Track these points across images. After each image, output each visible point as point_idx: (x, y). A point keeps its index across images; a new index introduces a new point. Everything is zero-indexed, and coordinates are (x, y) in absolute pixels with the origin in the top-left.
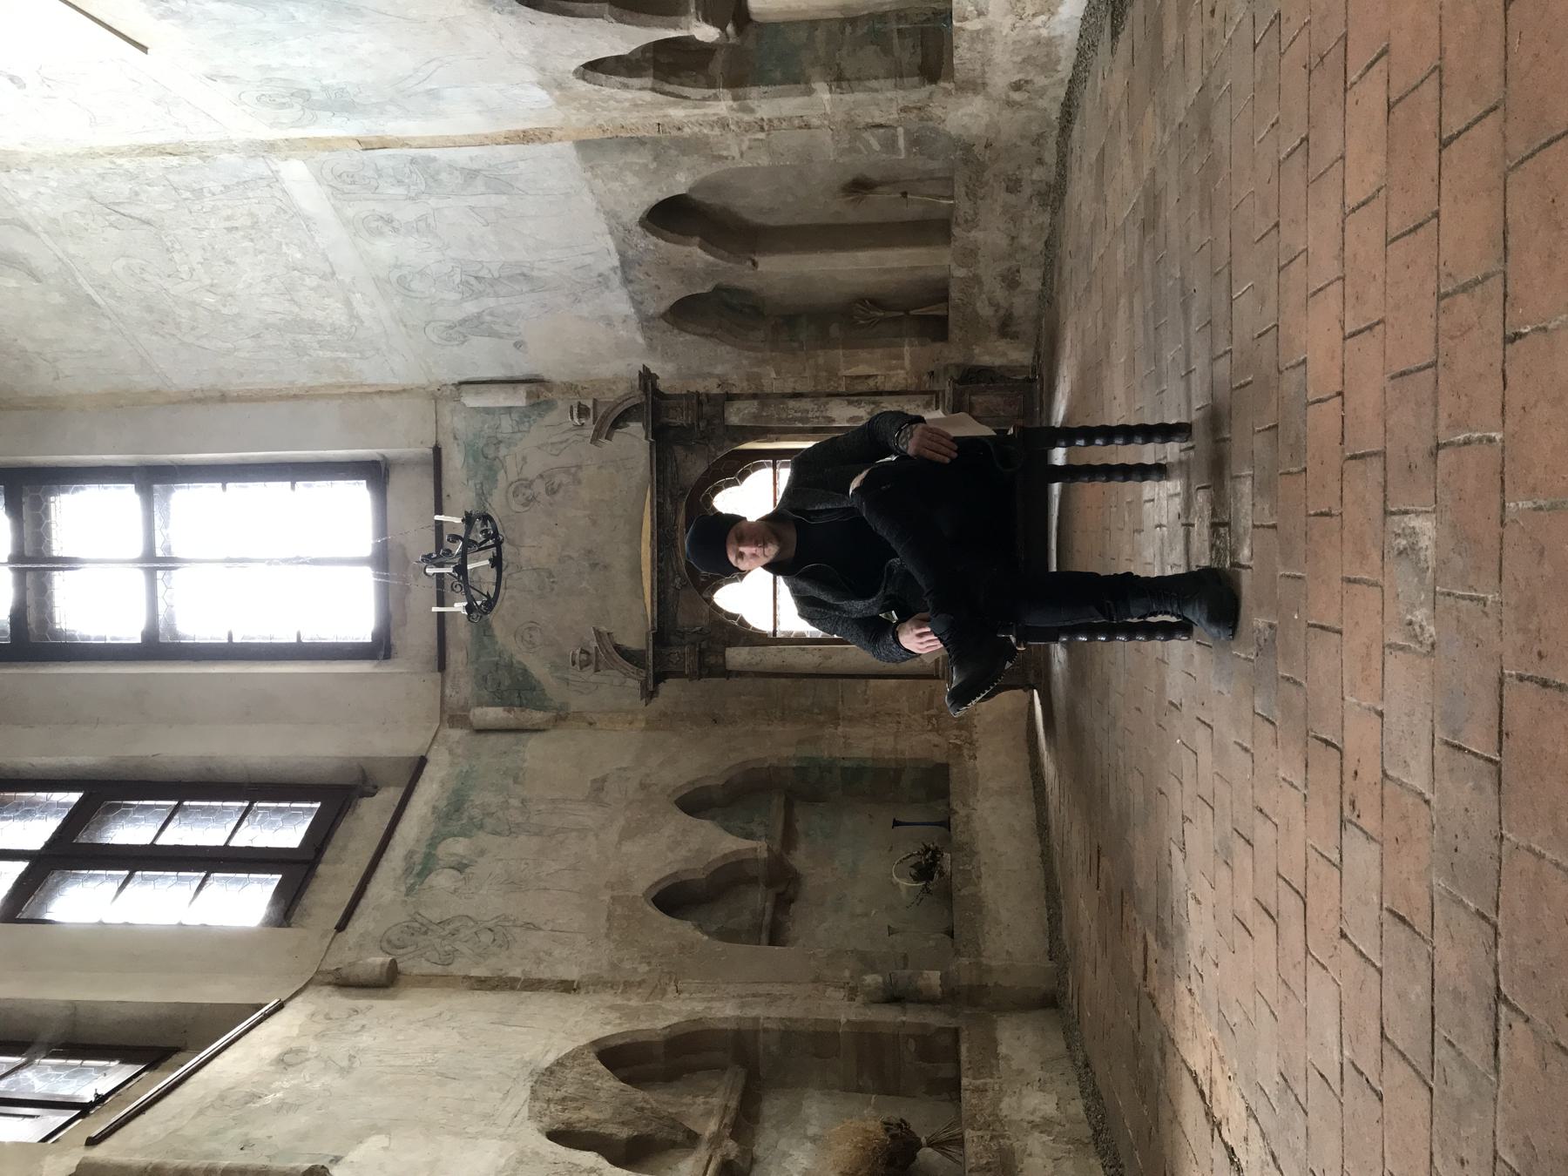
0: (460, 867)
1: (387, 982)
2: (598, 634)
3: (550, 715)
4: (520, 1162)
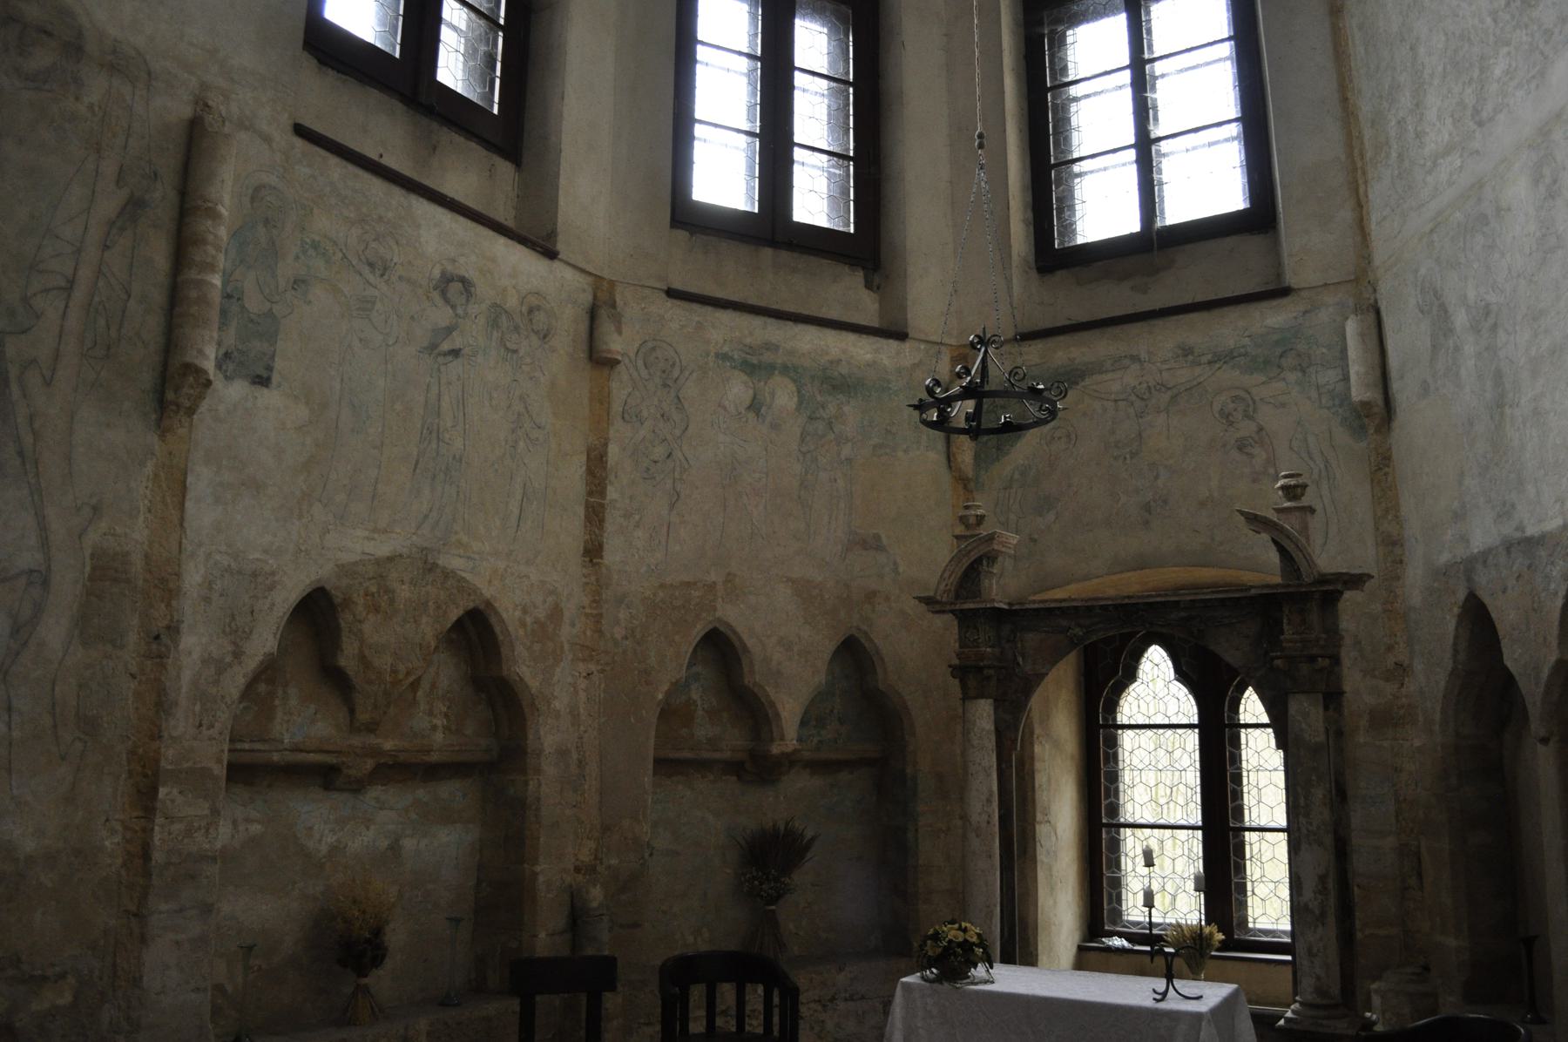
0: (755, 406)
3: (970, 472)
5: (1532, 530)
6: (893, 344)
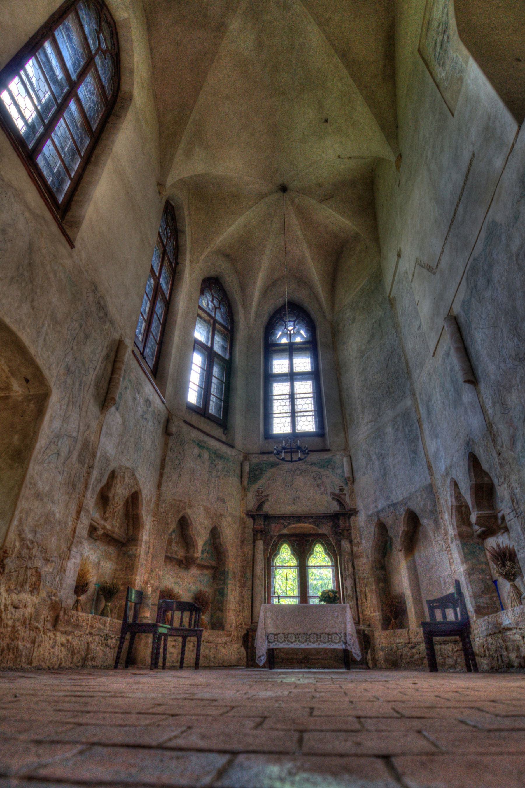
0: (199, 456)
1: (167, 433)
2: (268, 496)
4: (107, 460)
5: (395, 501)
6: (231, 449)
